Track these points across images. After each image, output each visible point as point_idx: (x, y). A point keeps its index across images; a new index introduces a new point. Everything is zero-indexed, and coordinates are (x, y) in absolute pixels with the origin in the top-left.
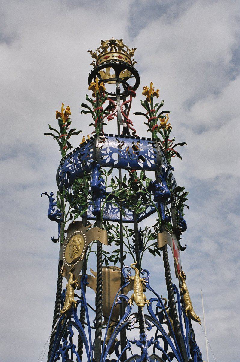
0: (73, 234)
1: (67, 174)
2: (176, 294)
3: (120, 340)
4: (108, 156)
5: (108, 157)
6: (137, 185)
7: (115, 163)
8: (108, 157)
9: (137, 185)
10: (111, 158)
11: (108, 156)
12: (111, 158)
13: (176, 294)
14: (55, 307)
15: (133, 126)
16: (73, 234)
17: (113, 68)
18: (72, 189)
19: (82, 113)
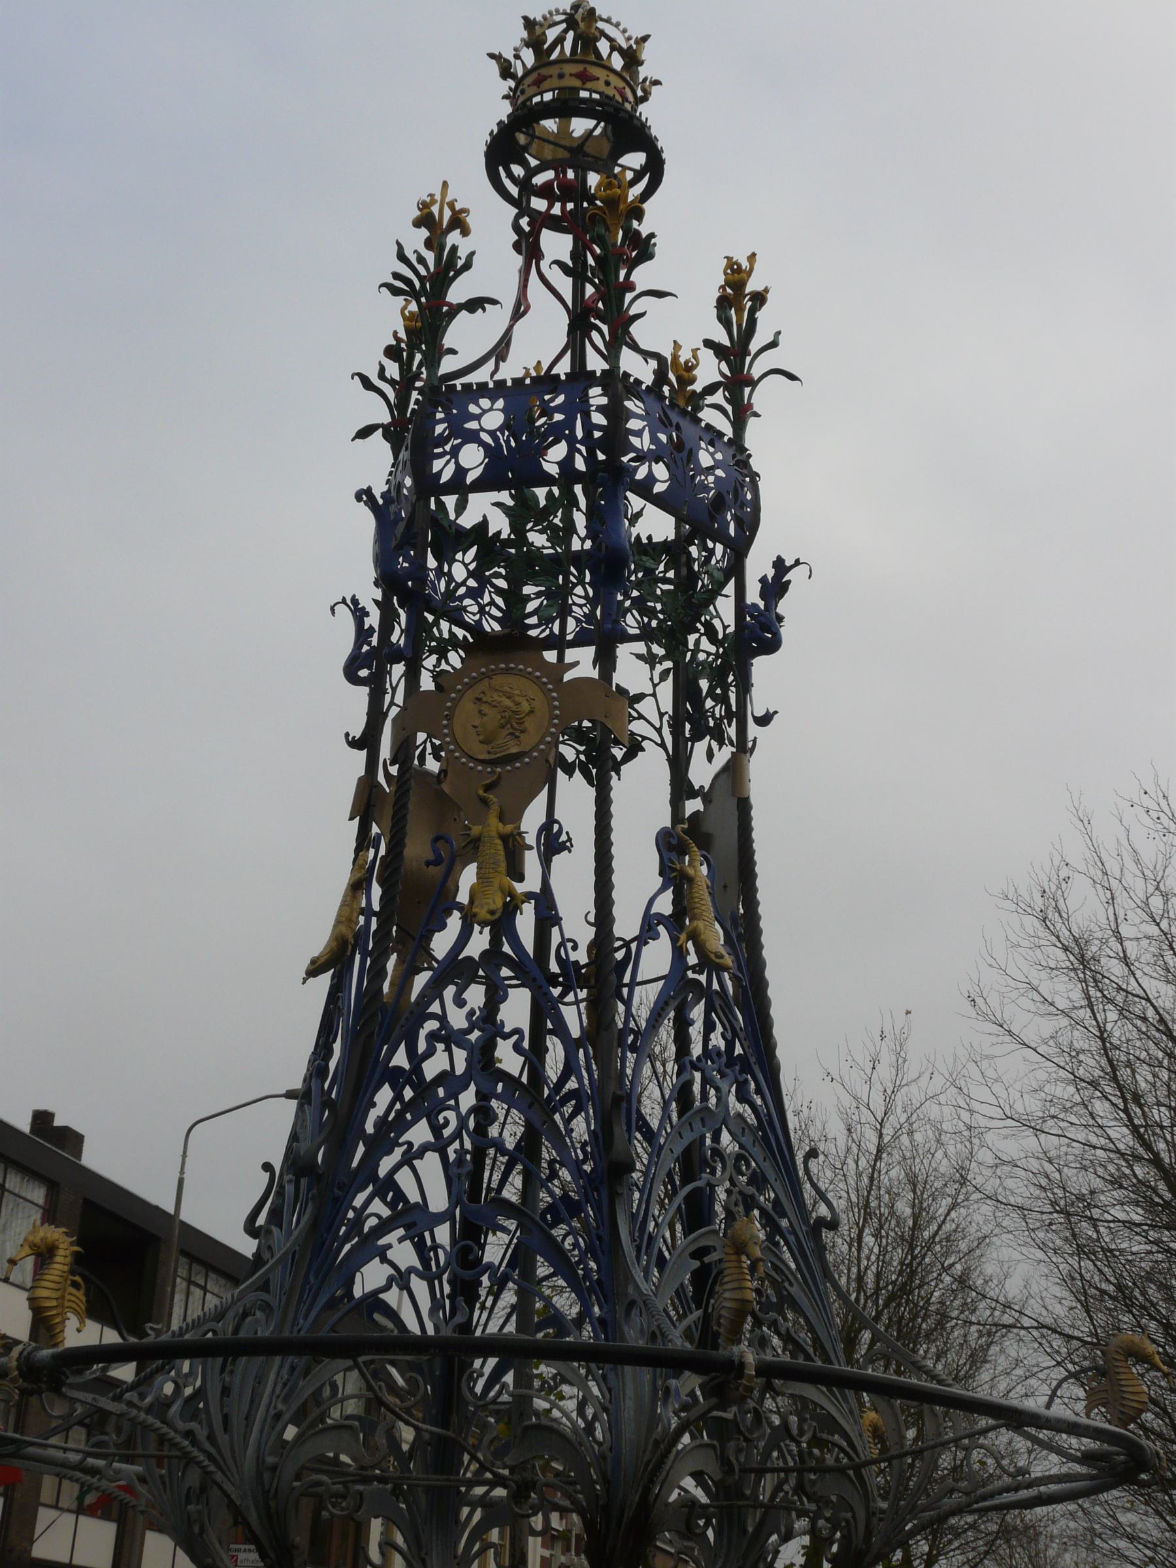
0: (503, 666)
1: (355, 1164)
2: (749, 601)
3: (468, 527)
4: (448, 457)
5: (448, 462)
6: (395, 774)
7: (471, 477)
8: (448, 462)
9: (395, 774)
10: (457, 463)
11: (448, 457)
12: (457, 463)
13: (749, 601)
14: (393, 818)
15: (498, 505)
16: (503, 666)
17: (622, 155)
18: (707, 450)
19: (384, 289)
